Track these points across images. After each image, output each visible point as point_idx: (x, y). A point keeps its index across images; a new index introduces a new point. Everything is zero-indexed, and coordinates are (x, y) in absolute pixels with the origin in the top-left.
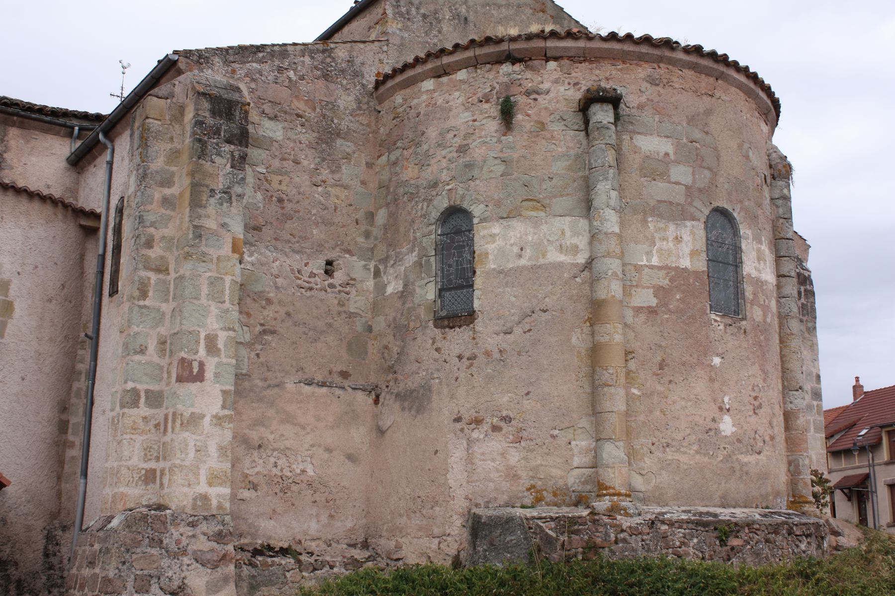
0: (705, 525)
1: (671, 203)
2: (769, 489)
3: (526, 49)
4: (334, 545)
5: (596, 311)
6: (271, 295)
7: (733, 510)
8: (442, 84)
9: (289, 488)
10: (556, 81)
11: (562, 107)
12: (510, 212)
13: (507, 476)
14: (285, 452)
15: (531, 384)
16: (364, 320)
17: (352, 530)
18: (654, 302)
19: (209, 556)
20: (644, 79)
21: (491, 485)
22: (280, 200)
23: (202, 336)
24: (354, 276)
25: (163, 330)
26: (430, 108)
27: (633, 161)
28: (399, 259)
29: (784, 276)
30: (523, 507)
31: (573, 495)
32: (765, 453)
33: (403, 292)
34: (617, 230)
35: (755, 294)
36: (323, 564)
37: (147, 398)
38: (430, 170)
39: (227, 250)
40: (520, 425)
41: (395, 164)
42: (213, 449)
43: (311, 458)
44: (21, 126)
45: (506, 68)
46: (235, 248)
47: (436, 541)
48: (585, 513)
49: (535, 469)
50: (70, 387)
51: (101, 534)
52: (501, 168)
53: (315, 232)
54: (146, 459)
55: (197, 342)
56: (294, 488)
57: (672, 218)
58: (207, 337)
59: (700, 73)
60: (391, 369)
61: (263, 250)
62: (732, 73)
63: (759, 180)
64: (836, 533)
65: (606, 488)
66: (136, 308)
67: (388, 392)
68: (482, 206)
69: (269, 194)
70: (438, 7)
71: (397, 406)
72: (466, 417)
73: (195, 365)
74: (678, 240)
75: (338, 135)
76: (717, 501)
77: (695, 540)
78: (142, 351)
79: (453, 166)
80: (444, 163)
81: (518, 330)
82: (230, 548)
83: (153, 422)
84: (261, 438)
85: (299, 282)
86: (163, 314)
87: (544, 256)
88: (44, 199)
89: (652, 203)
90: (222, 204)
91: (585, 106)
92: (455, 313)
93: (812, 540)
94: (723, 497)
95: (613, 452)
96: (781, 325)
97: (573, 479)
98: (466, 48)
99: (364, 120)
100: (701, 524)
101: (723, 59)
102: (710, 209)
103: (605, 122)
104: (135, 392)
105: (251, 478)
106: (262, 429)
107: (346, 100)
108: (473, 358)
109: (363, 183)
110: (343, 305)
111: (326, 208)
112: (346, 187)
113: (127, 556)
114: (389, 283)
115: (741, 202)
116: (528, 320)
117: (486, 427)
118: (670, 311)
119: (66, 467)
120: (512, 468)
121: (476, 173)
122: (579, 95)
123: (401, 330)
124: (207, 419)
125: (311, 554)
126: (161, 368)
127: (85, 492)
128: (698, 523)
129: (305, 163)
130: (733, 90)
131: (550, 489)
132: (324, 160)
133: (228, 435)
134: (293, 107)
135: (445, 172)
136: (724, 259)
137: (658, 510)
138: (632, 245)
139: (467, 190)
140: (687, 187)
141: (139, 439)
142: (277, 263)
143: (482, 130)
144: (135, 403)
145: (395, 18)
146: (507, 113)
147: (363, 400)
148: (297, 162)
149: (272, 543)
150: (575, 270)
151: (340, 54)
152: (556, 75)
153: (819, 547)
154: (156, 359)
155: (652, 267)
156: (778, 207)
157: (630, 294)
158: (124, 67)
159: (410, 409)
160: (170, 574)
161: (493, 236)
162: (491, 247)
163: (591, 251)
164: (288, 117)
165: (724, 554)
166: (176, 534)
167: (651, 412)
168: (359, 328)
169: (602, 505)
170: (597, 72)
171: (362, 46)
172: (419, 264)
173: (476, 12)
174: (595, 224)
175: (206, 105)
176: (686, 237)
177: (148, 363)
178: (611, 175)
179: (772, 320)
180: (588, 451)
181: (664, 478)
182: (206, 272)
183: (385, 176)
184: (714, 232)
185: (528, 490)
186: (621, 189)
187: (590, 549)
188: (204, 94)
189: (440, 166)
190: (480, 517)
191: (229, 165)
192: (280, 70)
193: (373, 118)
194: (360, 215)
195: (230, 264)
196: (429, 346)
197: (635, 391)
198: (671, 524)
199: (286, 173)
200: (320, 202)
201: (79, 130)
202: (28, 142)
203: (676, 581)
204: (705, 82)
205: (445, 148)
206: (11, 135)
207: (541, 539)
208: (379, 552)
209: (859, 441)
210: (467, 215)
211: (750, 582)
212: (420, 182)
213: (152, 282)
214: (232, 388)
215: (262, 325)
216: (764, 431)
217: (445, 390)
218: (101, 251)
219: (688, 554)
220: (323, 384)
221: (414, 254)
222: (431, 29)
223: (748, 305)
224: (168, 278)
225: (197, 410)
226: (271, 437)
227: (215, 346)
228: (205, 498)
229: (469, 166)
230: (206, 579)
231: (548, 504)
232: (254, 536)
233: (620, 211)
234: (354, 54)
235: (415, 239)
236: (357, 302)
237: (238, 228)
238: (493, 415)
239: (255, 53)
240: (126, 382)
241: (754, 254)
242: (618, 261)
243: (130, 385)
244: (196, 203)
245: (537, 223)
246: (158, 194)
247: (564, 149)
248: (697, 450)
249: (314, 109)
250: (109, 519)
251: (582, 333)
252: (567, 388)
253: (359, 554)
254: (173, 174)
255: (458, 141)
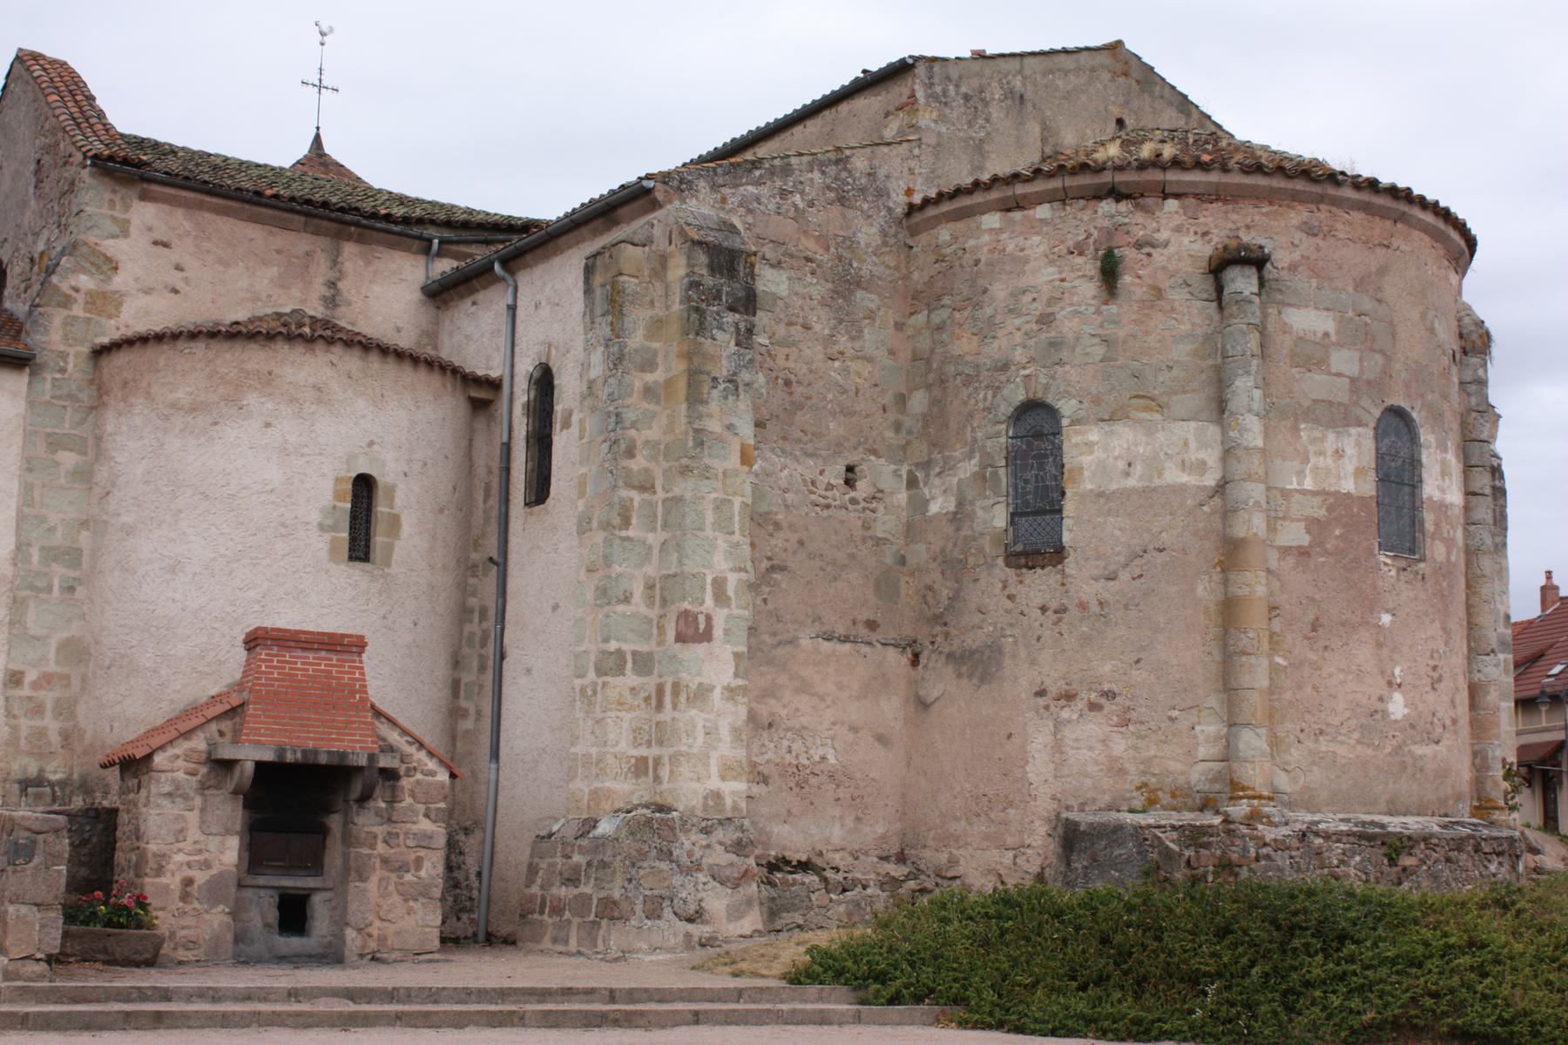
0: (1370, 838)
1: (1330, 403)
2: (1449, 791)
3: (1137, 183)
4: (862, 857)
5: (1231, 553)
6: (780, 517)
7: (1404, 820)
8: (1013, 221)
9: (806, 782)
10: (1178, 229)
11: (1186, 267)
12: (1113, 413)
13: (1110, 769)
14: (801, 732)
15: (1143, 648)
16: (894, 548)
17: (883, 837)
18: (1305, 540)
19: (728, 872)
20: (1297, 228)
21: (1088, 782)
22: (788, 383)
23: (709, 580)
24: (881, 486)
25: (651, 570)
26: (996, 255)
27: (1283, 345)
28: (948, 467)
29: (1475, 494)
30: (1131, 811)
31: (1198, 797)
32: (1445, 742)
33: (955, 513)
34: (1260, 443)
35: (1437, 525)
36: (856, 882)
37: (634, 662)
38: (996, 344)
39: (734, 461)
40: (1128, 703)
41: (940, 328)
42: (725, 733)
43: (833, 739)
44: (360, 240)
45: (1107, 206)
46: (746, 459)
47: (1011, 854)
48: (1217, 820)
49: (1148, 762)
50: (461, 631)
51: (584, 842)
52: (1100, 351)
53: (832, 425)
54: (637, 745)
55: (703, 589)
56: (813, 781)
57: (1331, 424)
58: (715, 581)
59: (1373, 215)
60: (938, 619)
61: (768, 455)
62: (1417, 212)
63: (1446, 361)
64: (1534, 851)
65: (1243, 789)
66: (618, 541)
67: (933, 651)
68: (1074, 402)
69: (774, 374)
70: (984, 81)
71: (950, 669)
72: (1053, 690)
73: (702, 619)
74: (1339, 454)
75: (858, 284)
76: (1383, 806)
77: (1358, 858)
78: (627, 599)
79: (1032, 342)
80: (1018, 337)
81: (1125, 576)
82: (751, 861)
83: (643, 695)
84: (773, 714)
85: (813, 497)
86: (650, 548)
87: (1160, 475)
88: (400, 355)
89: (1306, 403)
90: (726, 398)
91: (1219, 267)
92: (1035, 547)
93: (1505, 860)
94: (1391, 801)
95: (1252, 742)
96: (1468, 563)
97: (1197, 776)
98: (1051, 175)
99: (890, 260)
100: (1366, 837)
101: (1405, 196)
102: (1382, 408)
103: (1247, 293)
104: (620, 654)
105: (760, 768)
106: (773, 702)
107: (868, 233)
108: (1062, 610)
109: (892, 352)
110: (869, 528)
111: (845, 392)
112: (869, 360)
113: (633, 872)
114: (933, 498)
115: (1422, 396)
116: (1138, 561)
117: (1080, 704)
118: (1326, 553)
119: (459, 744)
120: (1116, 759)
121: (1065, 354)
122: (1208, 250)
123: (955, 567)
124: (717, 691)
125: (837, 870)
126: (650, 621)
127: (497, 780)
128: (1362, 836)
129: (817, 327)
130: (1416, 234)
131: (1167, 789)
132: (841, 321)
133: (743, 712)
134: (801, 247)
135: (1019, 350)
136: (1398, 474)
137: (1309, 818)
138: (1278, 462)
139: (1053, 378)
140: (1353, 380)
141: (627, 716)
142: (786, 472)
143: (1073, 294)
144: (620, 670)
145: (928, 104)
146: (1109, 272)
147: (896, 660)
148: (807, 327)
149: (788, 854)
150: (1202, 496)
151: (859, 164)
152: (1178, 220)
153: (1514, 868)
154: (643, 610)
155: (1304, 492)
156: (1469, 395)
157: (1275, 530)
158: (323, 34)
159: (970, 676)
160: (684, 895)
161: (1090, 445)
162: (1086, 460)
163: (1224, 468)
164: (795, 263)
165: (1393, 876)
166: (688, 843)
167: (1300, 688)
168: (889, 560)
169: (1240, 810)
170: (1235, 217)
171: (885, 149)
172: (980, 477)
173: (1035, 84)
174: (1231, 434)
175: (702, 258)
176: (1350, 450)
177: (635, 615)
178: (1254, 368)
179: (1458, 557)
180: (1217, 738)
181: (1316, 776)
182: (710, 492)
183: (924, 343)
184: (1386, 441)
185: (1138, 788)
186: (1265, 385)
187: (1224, 867)
188: (700, 243)
189: (1011, 341)
190: (1076, 824)
191: (733, 343)
192: (783, 194)
193: (902, 257)
194: (888, 399)
195: (738, 480)
196: (997, 591)
197: (1280, 660)
198: (1327, 836)
199: (794, 344)
200: (837, 384)
201: (440, 243)
202: (368, 263)
203: (1347, 909)
204: (1380, 227)
205: (1020, 315)
206: (346, 254)
207: (1160, 853)
208: (923, 867)
209: (1548, 685)
210: (1052, 413)
211: (1435, 912)
212: (981, 360)
213: (636, 504)
214: (745, 649)
215: (769, 559)
216: (1445, 713)
217: (1023, 653)
218: (505, 439)
219: (1347, 876)
220: (845, 639)
221: (973, 462)
222: (976, 117)
223: (1428, 540)
224: (655, 498)
225: (705, 680)
226: (783, 712)
227: (724, 592)
228: (717, 796)
229: (1055, 345)
230: (725, 902)
231: (1164, 808)
232: (766, 845)
233: (1264, 416)
234: (876, 162)
235: (976, 441)
236: (887, 523)
237: (747, 431)
238: (1090, 689)
239: (750, 171)
240: (606, 640)
241: (1437, 468)
242: (1262, 487)
243: (613, 645)
244: (695, 399)
245: (1150, 431)
246: (638, 381)
247: (1188, 327)
248: (1362, 743)
249: (827, 249)
250: (594, 823)
251: (1210, 581)
252: (1189, 654)
253: (897, 871)
254: (655, 352)
255: (1039, 308)
